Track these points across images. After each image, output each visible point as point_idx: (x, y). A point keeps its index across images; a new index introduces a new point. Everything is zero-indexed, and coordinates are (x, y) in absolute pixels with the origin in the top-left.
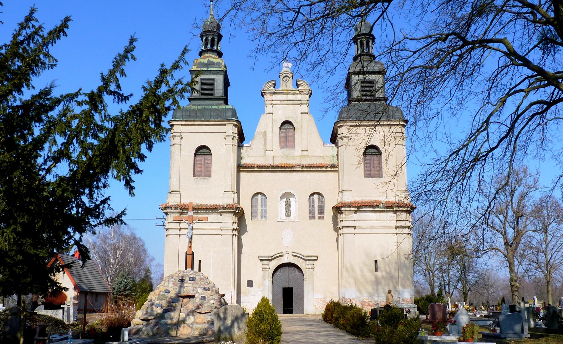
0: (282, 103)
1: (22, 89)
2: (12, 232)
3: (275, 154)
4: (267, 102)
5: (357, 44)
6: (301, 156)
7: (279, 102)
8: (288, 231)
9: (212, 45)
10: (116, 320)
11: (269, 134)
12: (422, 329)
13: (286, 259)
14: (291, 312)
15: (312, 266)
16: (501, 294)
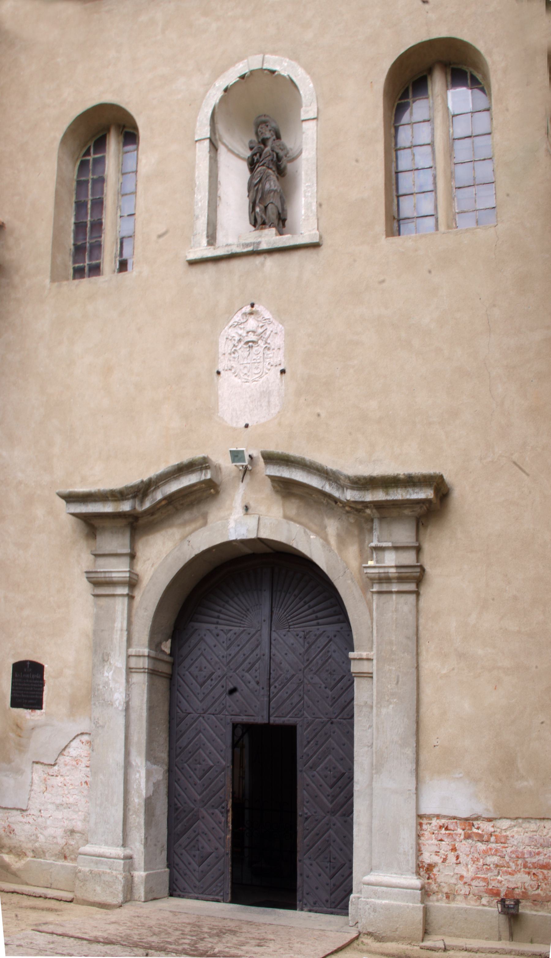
8: (252, 323)
15: (409, 558)
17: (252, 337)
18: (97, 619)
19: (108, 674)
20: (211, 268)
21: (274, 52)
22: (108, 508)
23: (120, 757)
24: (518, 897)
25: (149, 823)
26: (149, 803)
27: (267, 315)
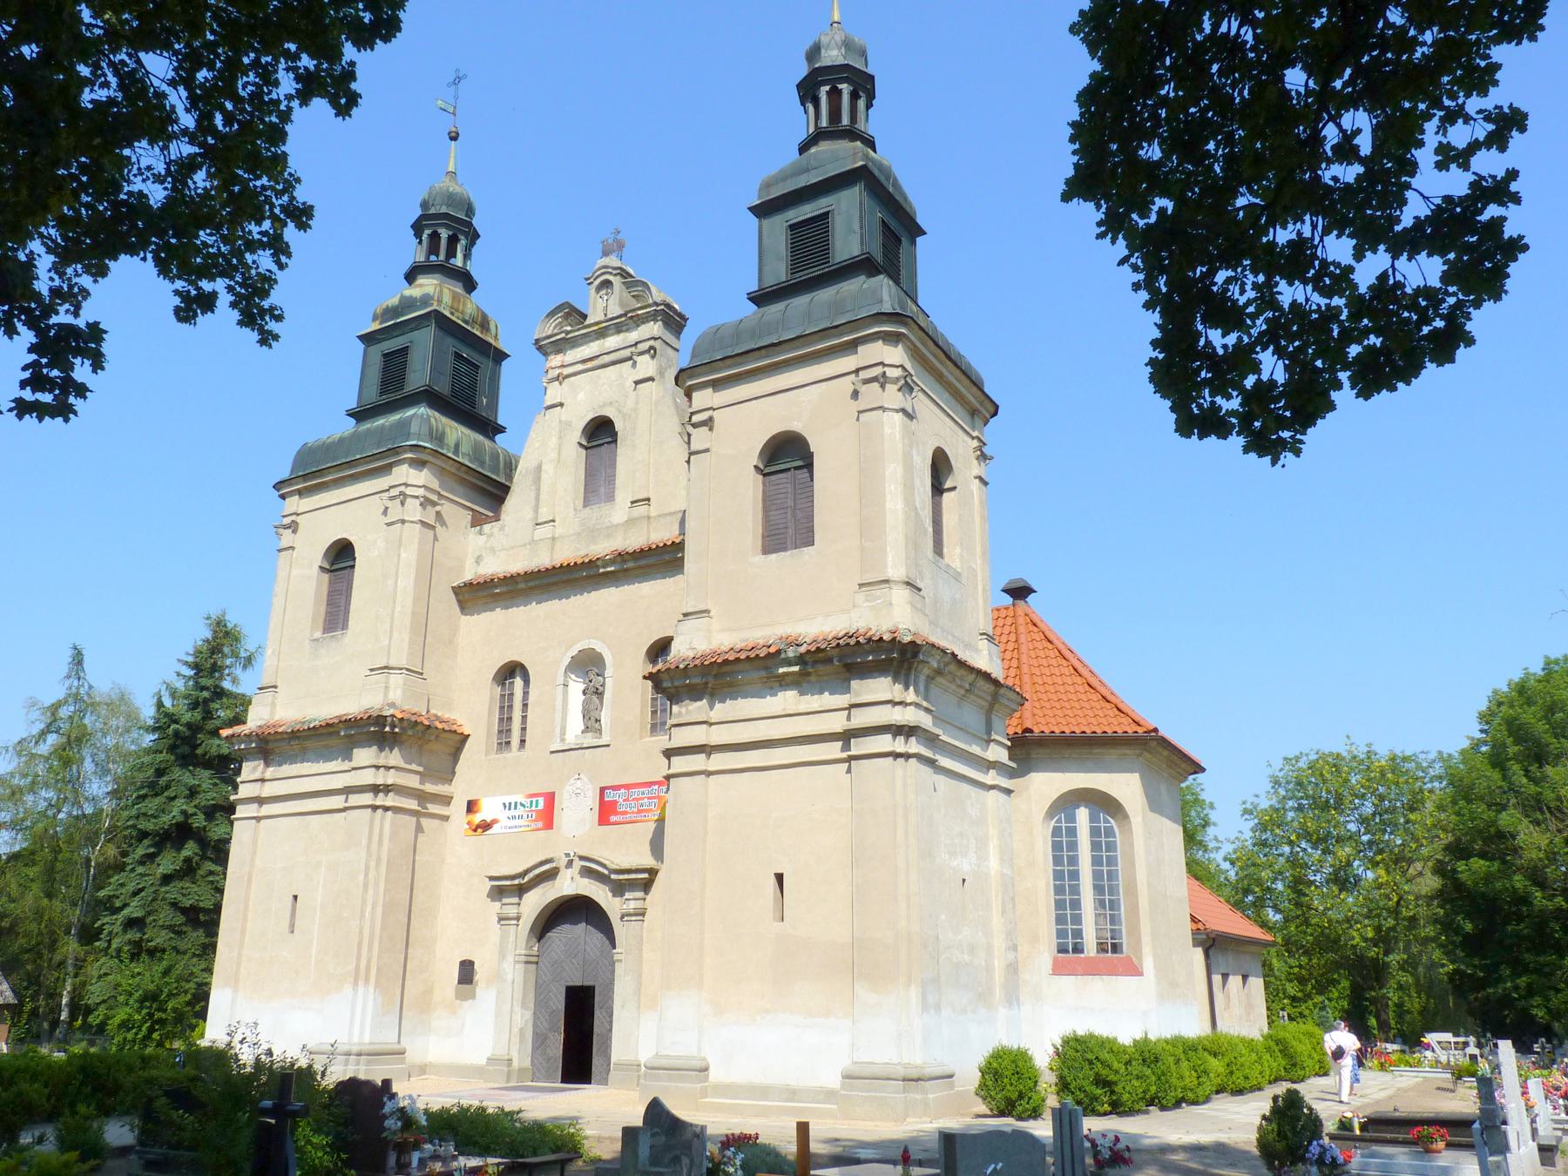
0: (589, 365)
1: (1509, 231)
2: (1327, 883)
3: (559, 531)
4: (1433, 207)
5: (816, 102)
6: (631, 522)
7: (580, 367)
9: (451, 253)
10: (455, 1110)
11: (548, 471)
12: (724, 1156)
13: (569, 884)
14: (798, 1124)
16: (1513, 1105)
17: (578, 791)
18: (502, 937)
19: (505, 965)
20: (561, 754)
21: (595, 638)
22: (508, 883)
23: (509, 1007)
24: (1268, 1037)
25: (521, 1042)
26: (521, 1030)
27: (586, 780)
